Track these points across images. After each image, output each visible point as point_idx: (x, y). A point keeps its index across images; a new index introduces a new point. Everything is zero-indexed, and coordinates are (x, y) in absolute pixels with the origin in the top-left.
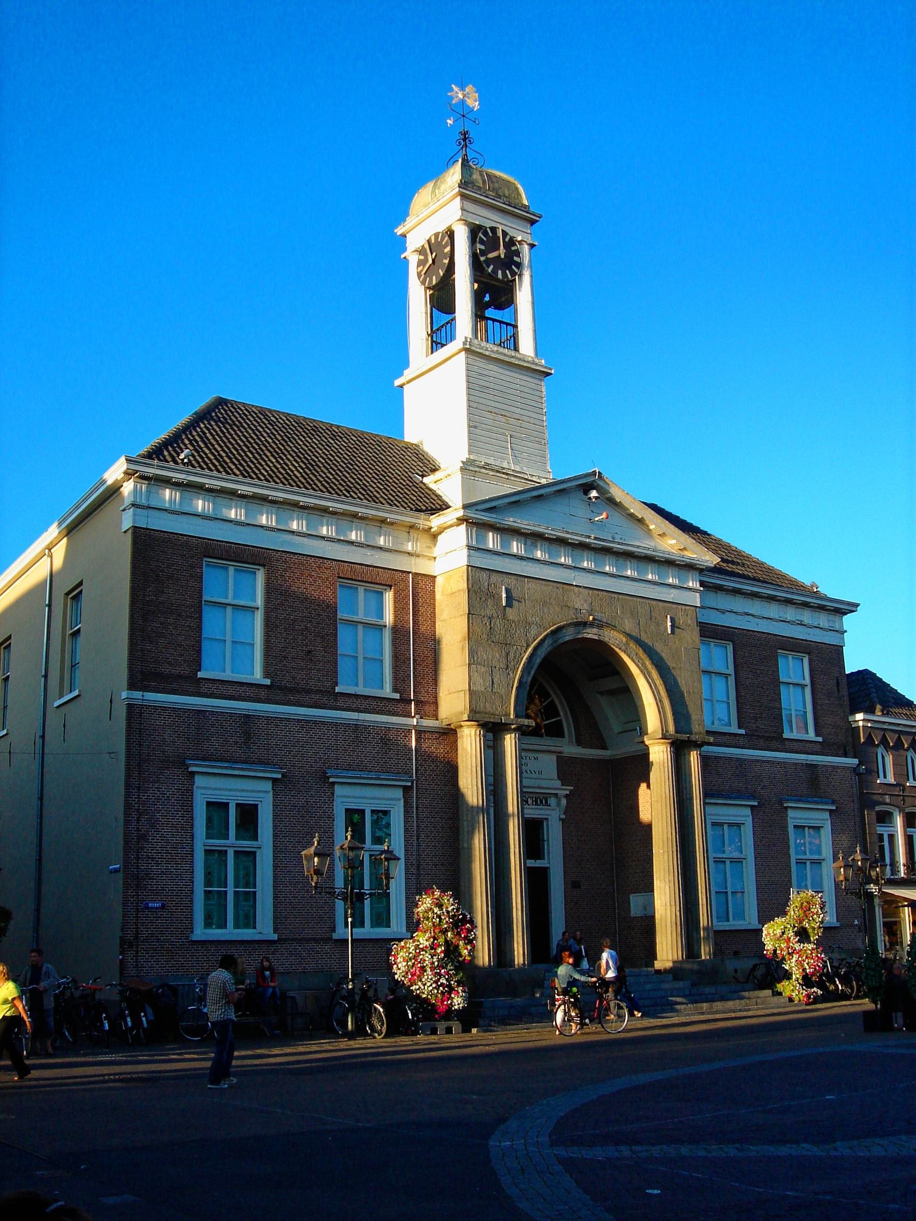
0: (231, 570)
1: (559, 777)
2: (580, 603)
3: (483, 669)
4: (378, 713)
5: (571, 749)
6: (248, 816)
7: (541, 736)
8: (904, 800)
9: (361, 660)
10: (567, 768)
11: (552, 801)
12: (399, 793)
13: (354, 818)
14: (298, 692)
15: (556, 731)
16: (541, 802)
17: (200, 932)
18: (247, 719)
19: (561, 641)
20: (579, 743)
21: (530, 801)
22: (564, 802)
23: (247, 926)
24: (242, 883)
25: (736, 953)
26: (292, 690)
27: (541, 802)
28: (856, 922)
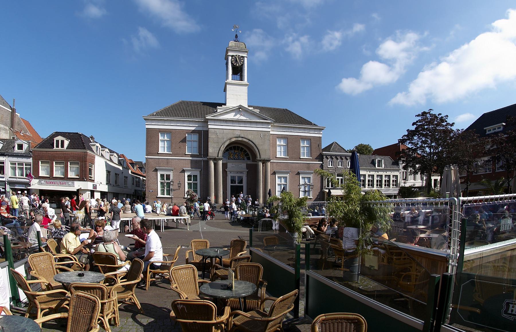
2: (238, 133)
5: (249, 162)
10: (248, 166)
11: (244, 173)
13: (162, 176)
17: (160, 195)
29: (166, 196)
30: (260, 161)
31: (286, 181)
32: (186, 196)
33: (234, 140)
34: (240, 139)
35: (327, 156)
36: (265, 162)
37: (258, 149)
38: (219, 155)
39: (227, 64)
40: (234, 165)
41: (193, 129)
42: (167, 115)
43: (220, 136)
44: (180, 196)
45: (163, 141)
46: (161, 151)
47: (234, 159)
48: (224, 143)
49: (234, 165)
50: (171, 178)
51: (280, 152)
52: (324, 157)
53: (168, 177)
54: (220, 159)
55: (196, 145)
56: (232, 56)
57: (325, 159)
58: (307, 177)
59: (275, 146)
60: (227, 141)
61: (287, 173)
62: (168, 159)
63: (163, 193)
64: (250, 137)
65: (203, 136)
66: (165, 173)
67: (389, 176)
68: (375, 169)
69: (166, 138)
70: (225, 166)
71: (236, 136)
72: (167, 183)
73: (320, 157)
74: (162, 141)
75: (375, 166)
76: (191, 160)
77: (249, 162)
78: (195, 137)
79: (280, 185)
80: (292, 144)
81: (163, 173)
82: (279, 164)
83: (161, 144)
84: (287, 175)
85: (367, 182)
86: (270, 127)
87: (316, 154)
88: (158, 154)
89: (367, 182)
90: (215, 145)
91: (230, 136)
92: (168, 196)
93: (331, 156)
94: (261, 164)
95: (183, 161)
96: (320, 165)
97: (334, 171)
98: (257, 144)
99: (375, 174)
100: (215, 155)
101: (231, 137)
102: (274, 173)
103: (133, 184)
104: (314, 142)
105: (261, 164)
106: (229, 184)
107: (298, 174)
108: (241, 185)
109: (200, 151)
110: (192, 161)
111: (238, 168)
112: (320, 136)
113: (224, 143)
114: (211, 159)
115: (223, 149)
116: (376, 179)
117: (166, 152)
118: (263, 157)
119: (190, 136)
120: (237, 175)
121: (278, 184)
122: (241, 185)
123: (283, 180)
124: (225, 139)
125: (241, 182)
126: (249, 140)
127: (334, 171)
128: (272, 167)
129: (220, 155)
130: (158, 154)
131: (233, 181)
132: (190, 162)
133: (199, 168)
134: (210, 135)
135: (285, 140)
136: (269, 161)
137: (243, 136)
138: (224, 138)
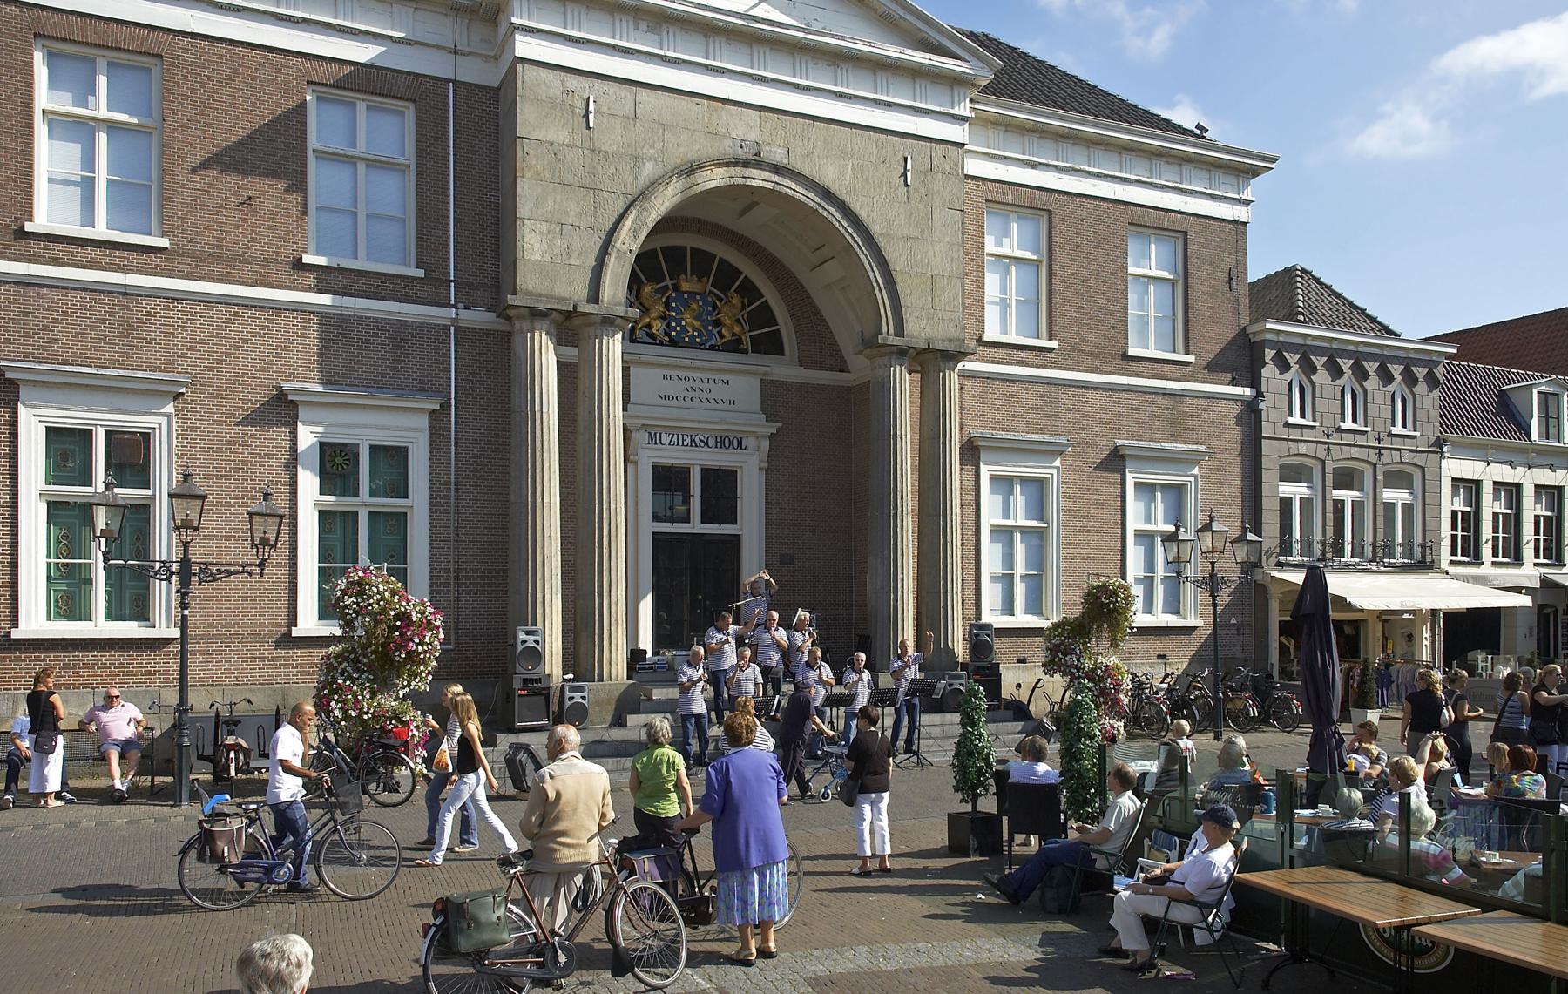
0: (361, 107)
1: (763, 410)
3: (545, 227)
4: (123, 271)
5: (784, 370)
6: (392, 459)
7: (745, 352)
8: (1380, 454)
9: (361, 217)
10: (774, 398)
11: (749, 442)
12: (423, 422)
13: (67, 448)
14: (228, 261)
15: (770, 345)
16: (731, 443)
17: (35, 620)
19: (699, 189)
20: (804, 362)
21: (711, 442)
22: (766, 444)
24: (339, 554)
25: (1021, 661)
26: (212, 259)
27: (731, 443)
28: (1233, 621)
29: (100, 626)
30: (902, 352)
31: (1038, 508)
32: (309, 623)
33: (714, 178)
34: (760, 179)
35: (1281, 348)
36: (932, 361)
38: (607, 293)
40: (677, 388)
41: (362, 53)
43: (611, 140)
44: (244, 627)
45: (79, 129)
46: (50, 212)
47: (674, 343)
48: (643, 195)
49: (677, 388)
51: (1004, 312)
52: (1269, 354)
53: (130, 457)
54: (609, 323)
55: (393, 195)
57: (1268, 371)
58: (1024, 480)
59: (974, 260)
61: (1046, 452)
62: (126, 292)
63: (69, 602)
64: (828, 174)
66: (101, 420)
67: (1512, 492)
68: (1525, 451)
69: (101, 107)
71: (728, 148)
73: (1242, 359)
74: (66, 126)
75: (1529, 435)
76: (326, 318)
77: (784, 370)
78: (388, 133)
79: (1004, 534)
80: (1079, 249)
81: (71, 416)
82: (998, 387)
83: (50, 157)
84: (1051, 470)
86: (963, 109)
87: (1216, 335)
88: (24, 240)
90: (573, 207)
91: (687, 147)
92: (129, 629)
93: (1306, 353)
95: (276, 320)
96: (1236, 409)
97: (1321, 452)
98: (876, 227)
99: (1529, 478)
100: (571, 289)
102: (972, 452)
104: (1202, 250)
105: (905, 385)
107: (1116, 461)
108: (727, 529)
109: (428, 248)
110: (332, 326)
111: (720, 402)
112: (1240, 213)
113: (643, 195)
114: (536, 314)
115: (629, 242)
117: (102, 230)
118: (921, 328)
119: (337, 114)
120: (697, 459)
121: (996, 531)
122: (727, 529)
123: (1019, 500)
124: (649, 170)
126: (827, 194)
127: (1321, 452)
129: (614, 289)
130: (24, 240)
132: (311, 332)
133: (421, 391)
134: (528, 119)
135: (1029, 227)
137: (777, 155)
138: (637, 160)
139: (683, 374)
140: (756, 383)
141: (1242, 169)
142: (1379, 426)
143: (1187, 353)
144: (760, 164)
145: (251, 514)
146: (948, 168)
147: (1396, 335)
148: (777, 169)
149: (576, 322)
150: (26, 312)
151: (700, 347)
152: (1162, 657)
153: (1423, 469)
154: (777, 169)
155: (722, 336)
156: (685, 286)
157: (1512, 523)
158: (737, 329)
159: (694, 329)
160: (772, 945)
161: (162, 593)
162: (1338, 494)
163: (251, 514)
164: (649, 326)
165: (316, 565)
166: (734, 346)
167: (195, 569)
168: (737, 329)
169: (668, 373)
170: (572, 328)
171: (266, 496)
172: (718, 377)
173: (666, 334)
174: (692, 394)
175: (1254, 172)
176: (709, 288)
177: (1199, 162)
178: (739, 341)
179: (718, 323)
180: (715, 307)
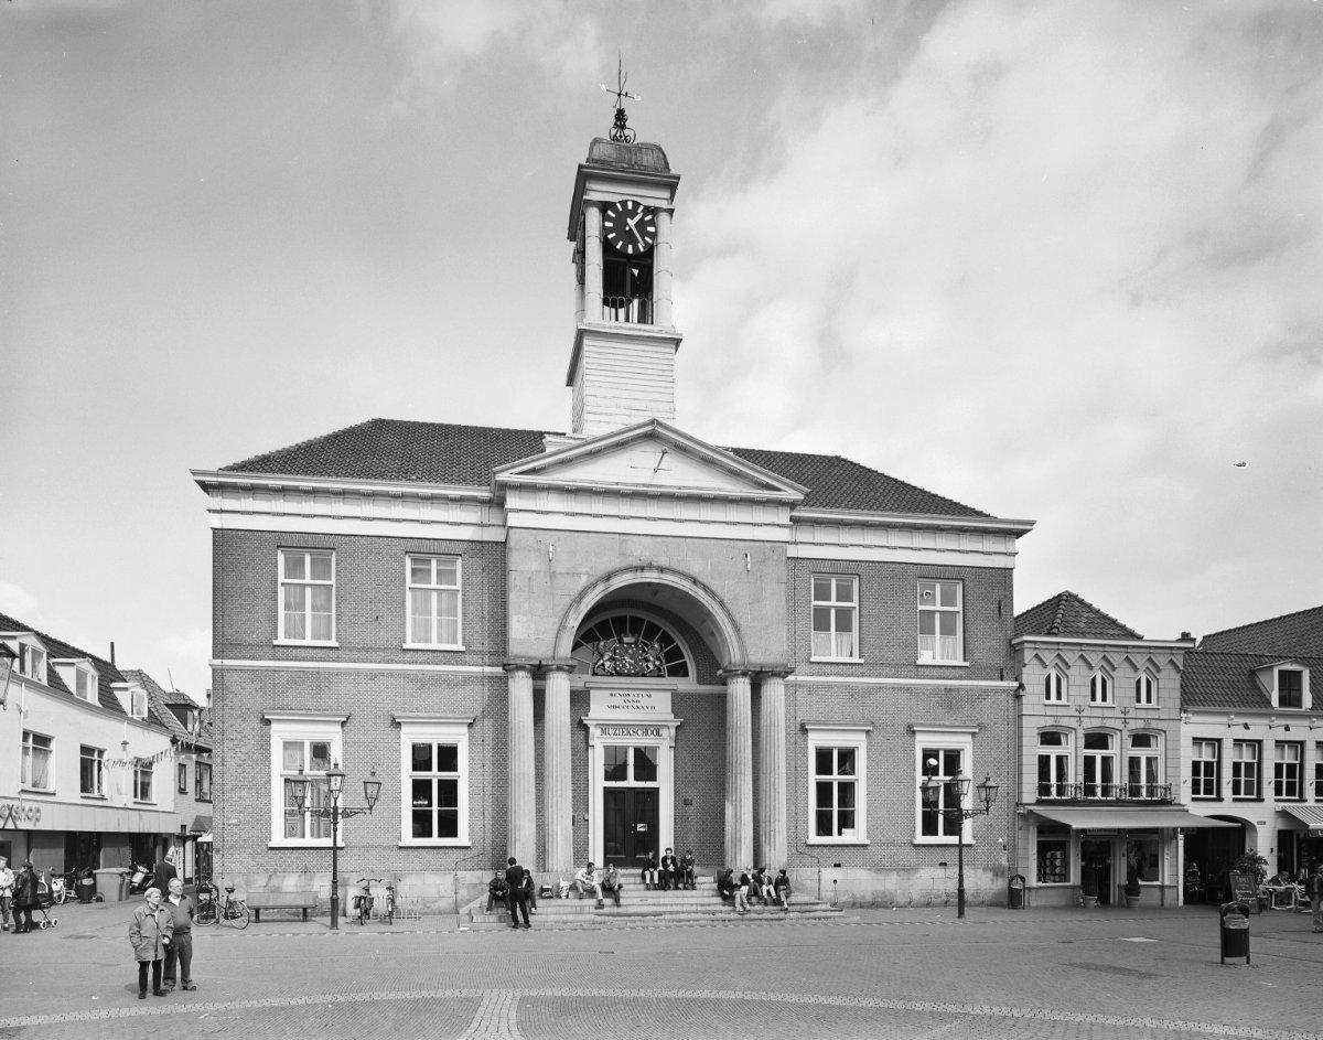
1: (673, 711)
2: (641, 552)
3: (525, 619)
10: (680, 702)
11: (664, 732)
15: (680, 671)
17: (278, 838)
18: (318, 672)
22: (673, 731)
23: (424, 836)
25: (837, 865)
28: (1001, 840)
36: (758, 679)
37: (732, 621)
39: (580, 255)
42: (308, 470)
47: (619, 674)
50: (336, 754)
56: (605, 207)
60: (592, 586)
63: (290, 832)
64: (695, 569)
65: (493, 557)
70: (579, 699)
71: (632, 561)
72: (839, 611)
85: (1269, 774)
89: (1269, 774)
94: (740, 689)
100: (539, 651)
101: (611, 567)
103: (182, 791)
105: (740, 689)
106: (598, 783)
116: (1270, 758)
124: (584, 580)
125: (646, 767)
128: (791, 704)
129: (565, 648)
131: (616, 772)
136: (783, 673)
137: (663, 561)
139: (622, 692)
140: (669, 695)
141: (1015, 532)
142: (1126, 703)
143: (965, 660)
144: (650, 567)
145: (365, 783)
146: (775, 558)
147: (1140, 638)
148: (661, 570)
149: (543, 669)
150: (274, 685)
151: (636, 675)
152: (945, 864)
153: (1165, 732)
154: (661, 570)
155: (648, 668)
156: (626, 640)
157: (1253, 770)
158: (657, 663)
159: (630, 664)
160: (31, 861)
161: (967, 825)
162: (1090, 752)
163: (365, 783)
164: (603, 665)
165: (458, 808)
166: (658, 673)
167: (340, 811)
168: (657, 663)
169: (614, 692)
170: (539, 672)
171: (373, 774)
172: (644, 693)
173: (615, 669)
174: (628, 704)
175: (1019, 534)
176: (641, 638)
177: (972, 531)
178: (659, 670)
179: (647, 660)
180: (644, 651)
